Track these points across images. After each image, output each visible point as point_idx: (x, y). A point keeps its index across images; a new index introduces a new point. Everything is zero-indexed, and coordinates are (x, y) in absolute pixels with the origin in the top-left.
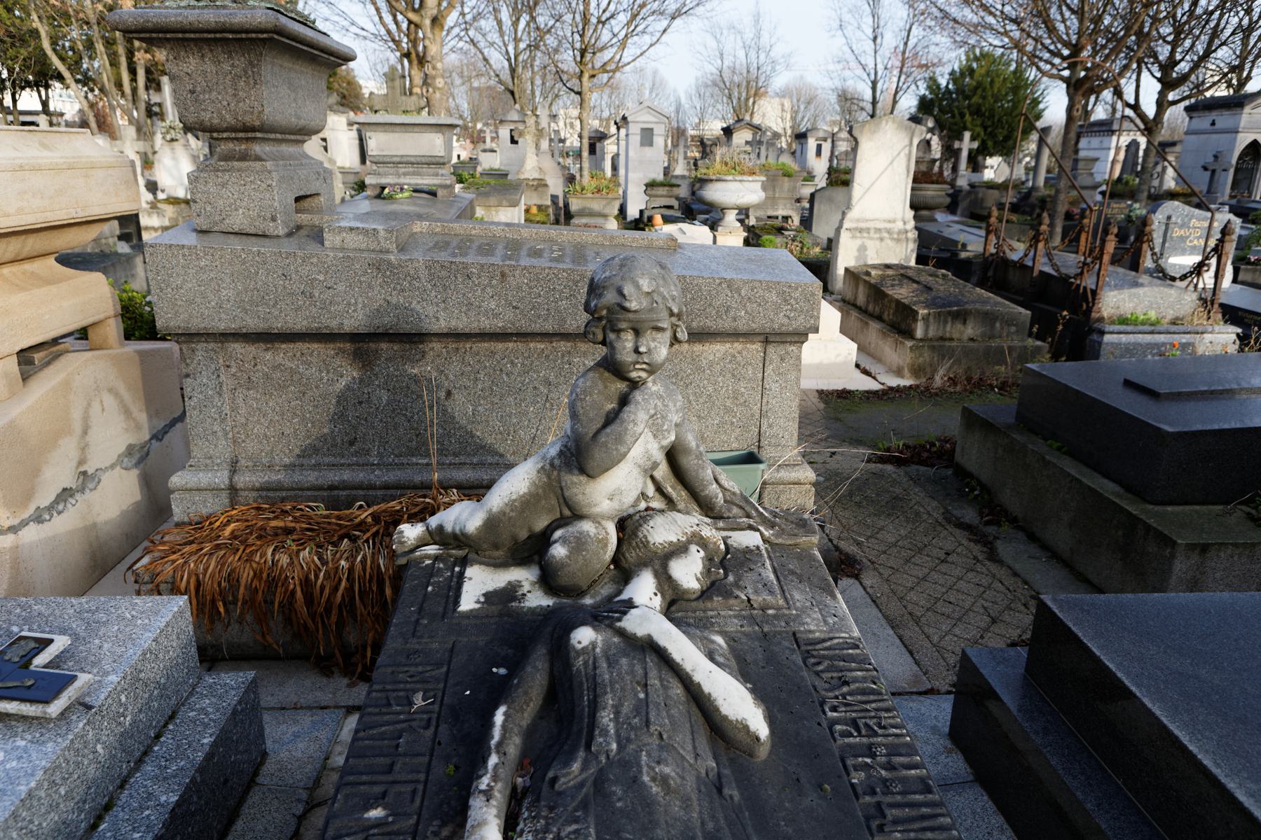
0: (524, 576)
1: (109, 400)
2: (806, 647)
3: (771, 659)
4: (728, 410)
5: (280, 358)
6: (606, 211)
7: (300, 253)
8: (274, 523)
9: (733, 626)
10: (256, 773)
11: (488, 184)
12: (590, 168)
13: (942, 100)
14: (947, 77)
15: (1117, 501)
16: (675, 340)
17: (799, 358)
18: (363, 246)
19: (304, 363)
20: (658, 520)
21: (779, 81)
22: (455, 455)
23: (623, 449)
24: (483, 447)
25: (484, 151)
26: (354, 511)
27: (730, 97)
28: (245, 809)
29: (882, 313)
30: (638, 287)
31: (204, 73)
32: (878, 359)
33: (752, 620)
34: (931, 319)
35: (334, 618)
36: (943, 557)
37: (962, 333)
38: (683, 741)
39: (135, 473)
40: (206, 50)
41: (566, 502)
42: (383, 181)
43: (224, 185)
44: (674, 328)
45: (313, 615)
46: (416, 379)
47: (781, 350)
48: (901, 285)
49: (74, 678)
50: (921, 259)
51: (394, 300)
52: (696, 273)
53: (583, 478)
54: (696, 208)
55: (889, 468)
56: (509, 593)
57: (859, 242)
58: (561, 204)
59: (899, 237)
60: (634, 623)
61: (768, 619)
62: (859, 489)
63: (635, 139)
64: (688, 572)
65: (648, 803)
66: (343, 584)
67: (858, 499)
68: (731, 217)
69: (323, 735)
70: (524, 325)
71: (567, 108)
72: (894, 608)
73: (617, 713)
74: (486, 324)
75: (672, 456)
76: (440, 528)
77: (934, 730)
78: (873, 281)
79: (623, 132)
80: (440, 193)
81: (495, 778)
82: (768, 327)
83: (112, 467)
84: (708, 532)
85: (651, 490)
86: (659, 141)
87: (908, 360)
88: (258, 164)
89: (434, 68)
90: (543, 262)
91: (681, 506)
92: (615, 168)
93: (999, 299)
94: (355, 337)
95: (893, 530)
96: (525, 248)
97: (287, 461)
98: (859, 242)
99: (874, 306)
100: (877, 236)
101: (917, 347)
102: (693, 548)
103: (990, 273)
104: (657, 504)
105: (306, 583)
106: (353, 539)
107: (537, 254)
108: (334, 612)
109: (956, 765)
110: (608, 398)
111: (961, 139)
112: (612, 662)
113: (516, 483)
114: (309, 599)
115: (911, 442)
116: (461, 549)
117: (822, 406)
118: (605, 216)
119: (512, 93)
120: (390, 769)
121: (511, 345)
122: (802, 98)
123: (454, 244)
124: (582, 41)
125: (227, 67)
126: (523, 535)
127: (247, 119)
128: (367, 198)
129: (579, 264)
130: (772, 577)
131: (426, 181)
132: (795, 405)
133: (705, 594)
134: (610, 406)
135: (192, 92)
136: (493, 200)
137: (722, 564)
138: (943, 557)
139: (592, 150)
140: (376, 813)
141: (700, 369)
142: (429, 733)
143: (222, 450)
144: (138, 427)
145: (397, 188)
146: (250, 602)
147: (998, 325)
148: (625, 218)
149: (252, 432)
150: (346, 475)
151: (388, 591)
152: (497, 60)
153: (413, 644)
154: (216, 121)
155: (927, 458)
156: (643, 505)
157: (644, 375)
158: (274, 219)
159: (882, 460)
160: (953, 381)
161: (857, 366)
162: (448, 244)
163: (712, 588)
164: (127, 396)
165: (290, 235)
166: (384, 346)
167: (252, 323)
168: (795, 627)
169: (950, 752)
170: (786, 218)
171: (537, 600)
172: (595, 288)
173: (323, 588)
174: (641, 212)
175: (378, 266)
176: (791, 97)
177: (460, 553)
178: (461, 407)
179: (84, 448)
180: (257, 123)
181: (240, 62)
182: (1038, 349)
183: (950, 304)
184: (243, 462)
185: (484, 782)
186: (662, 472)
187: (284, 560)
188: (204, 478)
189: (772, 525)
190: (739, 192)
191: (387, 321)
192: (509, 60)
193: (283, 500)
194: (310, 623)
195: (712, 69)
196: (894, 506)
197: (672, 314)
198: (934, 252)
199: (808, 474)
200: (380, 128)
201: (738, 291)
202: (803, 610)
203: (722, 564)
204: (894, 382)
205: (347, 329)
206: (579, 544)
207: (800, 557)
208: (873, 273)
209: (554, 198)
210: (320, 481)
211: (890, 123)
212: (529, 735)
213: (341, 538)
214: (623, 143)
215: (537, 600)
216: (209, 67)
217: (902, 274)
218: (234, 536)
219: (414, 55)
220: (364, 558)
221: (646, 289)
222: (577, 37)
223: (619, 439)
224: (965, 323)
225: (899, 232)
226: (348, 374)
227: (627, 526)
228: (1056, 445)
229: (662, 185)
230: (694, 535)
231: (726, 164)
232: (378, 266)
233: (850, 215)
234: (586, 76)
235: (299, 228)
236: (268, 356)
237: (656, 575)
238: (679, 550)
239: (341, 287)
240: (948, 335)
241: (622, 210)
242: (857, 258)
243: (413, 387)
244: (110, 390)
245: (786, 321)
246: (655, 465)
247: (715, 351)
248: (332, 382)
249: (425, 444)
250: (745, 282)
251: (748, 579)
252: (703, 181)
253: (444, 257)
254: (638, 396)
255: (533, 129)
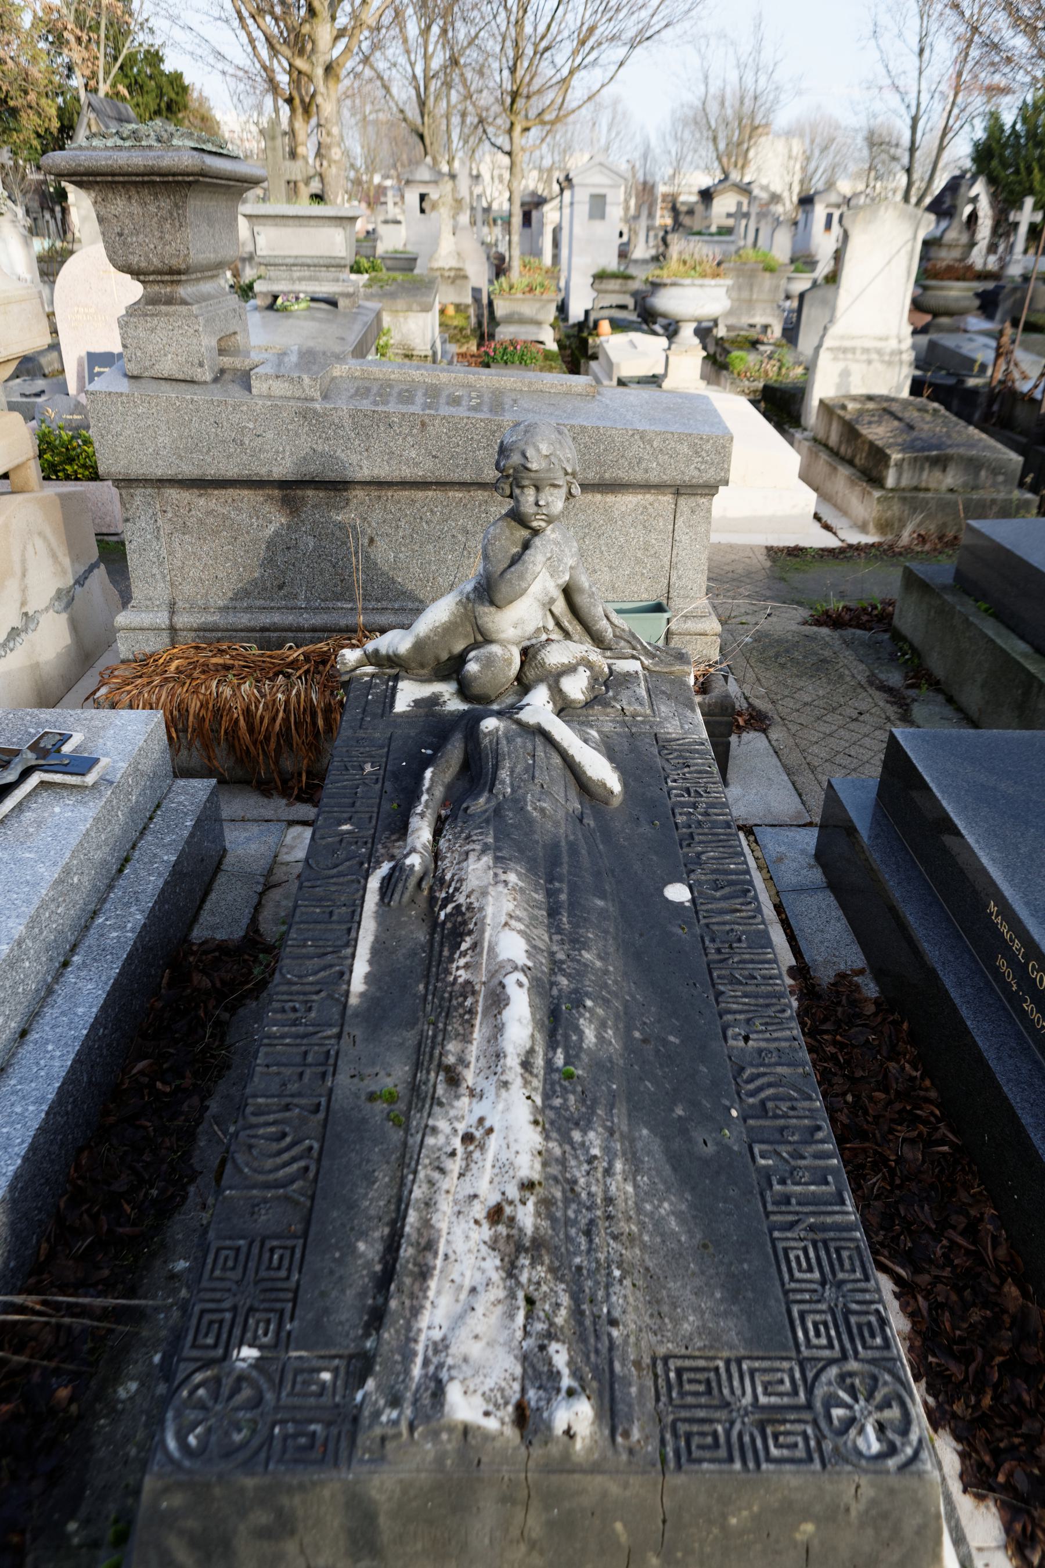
0: (446, 689)
1: (39, 543)
2: (662, 743)
3: (634, 749)
4: (638, 561)
5: (212, 504)
6: (540, 317)
7: (230, 401)
8: (214, 660)
9: (608, 727)
10: (220, 863)
11: (394, 280)
12: (523, 254)
13: (1005, 146)
14: (1015, 111)
15: (1021, 660)
16: (570, 495)
17: (709, 511)
18: (289, 394)
19: (236, 509)
20: (553, 647)
21: (782, 118)
22: (378, 600)
23: (524, 585)
24: (404, 593)
25: (386, 222)
26: (284, 651)
27: (715, 139)
28: (216, 886)
29: (854, 456)
30: (538, 450)
31: (131, 214)
32: (843, 511)
33: (624, 724)
34: (905, 466)
35: (273, 745)
36: (855, 715)
37: (940, 482)
38: (558, 791)
39: (64, 616)
40: (133, 192)
41: (479, 629)
42: (276, 288)
43: (153, 330)
44: (569, 485)
45: (255, 743)
46: (341, 526)
47: (692, 501)
48: (879, 423)
49: (96, 761)
50: (917, 387)
51: (320, 449)
52: (609, 424)
53: (493, 609)
54: (647, 317)
55: (825, 631)
56: (434, 700)
57: (841, 365)
58: (485, 301)
59: (891, 360)
60: (527, 716)
61: (636, 724)
62: (787, 651)
63: (583, 209)
64: (576, 687)
65: (530, 821)
66: (281, 714)
67: (782, 660)
68: (687, 331)
69: (272, 840)
70: (443, 474)
71: (490, 163)
72: (794, 758)
73: (512, 772)
74: (407, 473)
75: (567, 592)
76: (376, 652)
77: (803, 852)
78: (848, 417)
79: (567, 194)
80: (342, 303)
81: (427, 806)
82: (679, 479)
83: (47, 609)
84: (595, 656)
85: (551, 624)
86: (615, 212)
87: (874, 514)
88: (183, 309)
89: (329, 134)
90: (461, 412)
91: (576, 637)
92: (556, 244)
93: (992, 442)
94: (283, 484)
95: (811, 690)
96: (445, 393)
97: (220, 603)
98: (841, 365)
99: (847, 450)
100: (865, 357)
101: (886, 499)
102: (581, 669)
103: (995, 408)
104: (556, 635)
105: (248, 713)
106: (288, 676)
107: (455, 401)
108: (273, 740)
109: (817, 876)
110: (514, 543)
111: (1020, 208)
112: (510, 740)
113: (439, 613)
114: (251, 729)
115: (852, 605)
116: (394, 666)
117: (768, 564)
118: (538, 323)
119: (422, 137)
120: (353, 804)
121: (430, 493)
122: (820, 141)
123: (374, 390)
124: (514, 81)
125: (152, 209)
126: (444, 656)
127: (174, 263)
128: (256, 308)
129: (496, 413)
130: (644, 693)
131: (324, 289)
132: (704, 557)
133: (588, 704)
134: (515, 550)
135: (120, 235)
136: (400, 304)
137: (605, 684)
138: (855, 715)
139: (527, 220)
140: (346, 827)
141: (612, 520)
142: (378, 786)
143: (161, 592)
144: (64, 572)
145: (291, 296)
146: (199, 731)
147: (983, 473)
148: (566, 319)
149: (190, 574)
150: (277, 618)
151: (320, 722)
152: (403, 93)
153: (361, 734)
154: (143, 265)
155: (862, 622)
156: (544, 637)
157: (543, 524)
158: (201, 365)
159: (818, 623)
160: (922, 539)
161: (817, 517)
162: (368, 390)
163: (595, 700)
164: (48, 532)
165: (216, 380)
166: (310, 493)
167: (188, 470)
168: (656, 729)
169: (811, 867)
170: (766, 327)
171: (455, 705)
172: (503, 451)
173: (262, 718)
174: (587, 313)
175: (304, 415)
176: (802, 136)
177: (393, 671)
178: (384, 554)
179: (24, 590)
180: (183, 267)
181: (166, 203)
182: (1027, 503)
183: (930, 448)
184: (180, 604)
185: (419, 809)
186: (560, 606)
187: (228, 692)
188: (146, 619)
189: (653, 656)
190: (698, 298)
191: (313, 469)
192: (417, 89)
193: (219, 640)
194: (252, 748)
195: (692, 97)
196: (820, 667)
197: (566, 474)
198: (940, 379)
199: (713, 625)
200: (270, 221)
201: (650, 442)
202: (666, 719)
203: (605, 684)
204: (855, 538)
205: (276, 476)
206: (488, 662)
207: (672, 682)
208: (851, 406)
209: (476, 292)
210: (252, 623)
211: (890, 210)
212: (449, 788)
213: (276, 675)
214: (566, 211)
215: (455, 705)
216: (136, 208)
217: (885, 408)
218: (178, 671)
219: (297, 101)
220: (298, 694)
221: (545, 452)
222: (506, 73)
223: (521, 577)
224: (944, 470)
225: (892, 353)
226: (276, 520)
227: (527, 653)
228: (984, 606)
229: (614, 276)
230: (583, 659)
231: (685, 262)
232: (304, 415)
233: (834, 331)
234: (518, 129)
235: (222, 371)
236: (202, 502)
237: (550, 688)
238: (570, 669)
239: (270, 435)
240: (923, 485)
241: (562, 309)
242: (839, 386)
243: (338, 533)
244: (40, 534)
245: (696, 473)
246: (552, 601)
247: (628, 501)
248: (261, 528)
249: (350, 588)
250: (658, 434)
251: (625, 695)
252: (656, 286)
253: (366, 405)
254: (537, 541)
255: (449, 199)
